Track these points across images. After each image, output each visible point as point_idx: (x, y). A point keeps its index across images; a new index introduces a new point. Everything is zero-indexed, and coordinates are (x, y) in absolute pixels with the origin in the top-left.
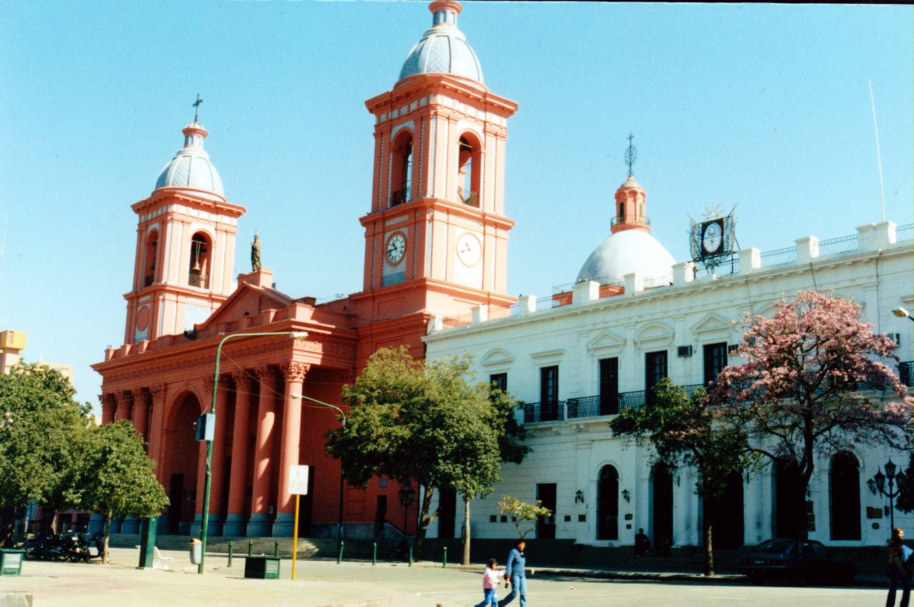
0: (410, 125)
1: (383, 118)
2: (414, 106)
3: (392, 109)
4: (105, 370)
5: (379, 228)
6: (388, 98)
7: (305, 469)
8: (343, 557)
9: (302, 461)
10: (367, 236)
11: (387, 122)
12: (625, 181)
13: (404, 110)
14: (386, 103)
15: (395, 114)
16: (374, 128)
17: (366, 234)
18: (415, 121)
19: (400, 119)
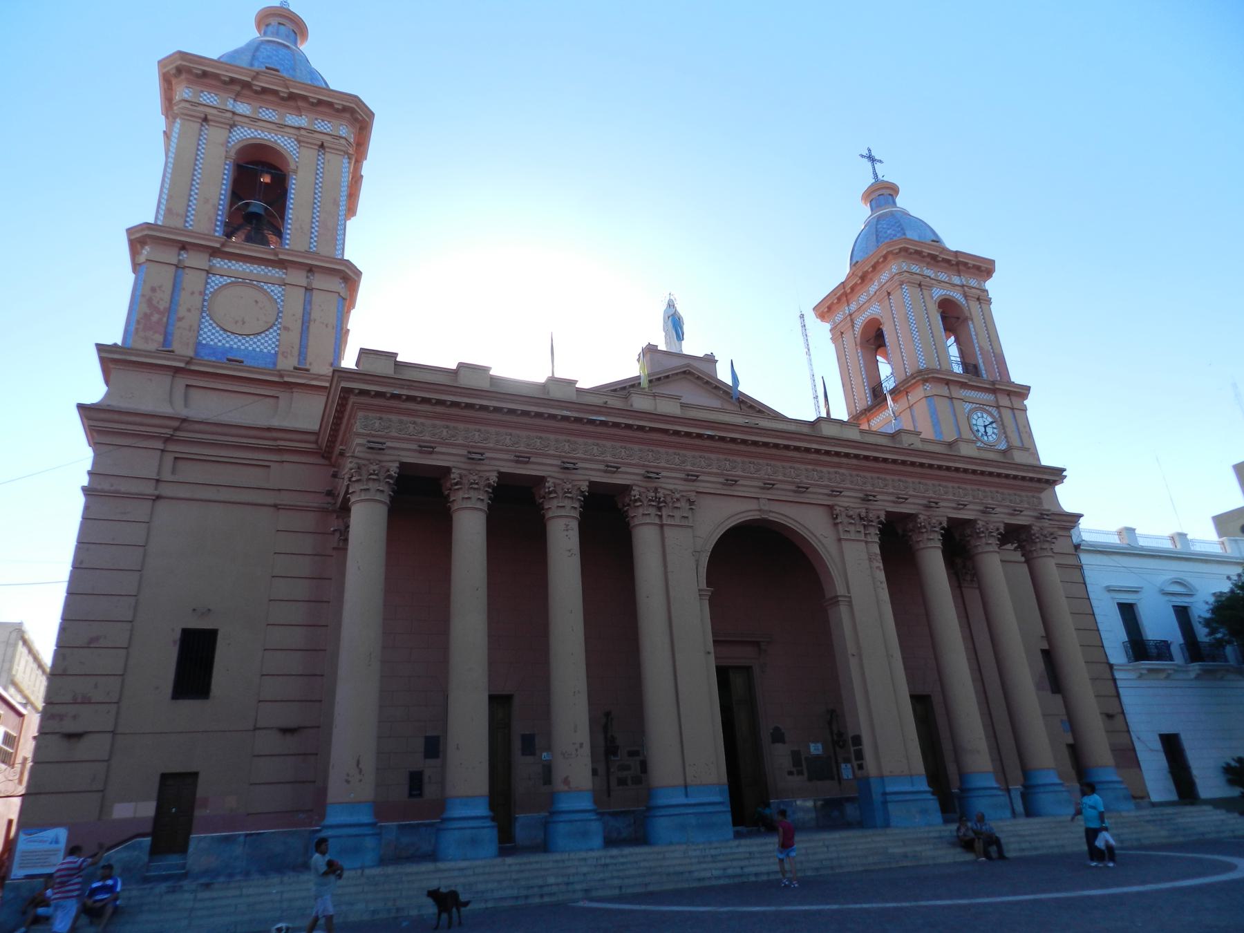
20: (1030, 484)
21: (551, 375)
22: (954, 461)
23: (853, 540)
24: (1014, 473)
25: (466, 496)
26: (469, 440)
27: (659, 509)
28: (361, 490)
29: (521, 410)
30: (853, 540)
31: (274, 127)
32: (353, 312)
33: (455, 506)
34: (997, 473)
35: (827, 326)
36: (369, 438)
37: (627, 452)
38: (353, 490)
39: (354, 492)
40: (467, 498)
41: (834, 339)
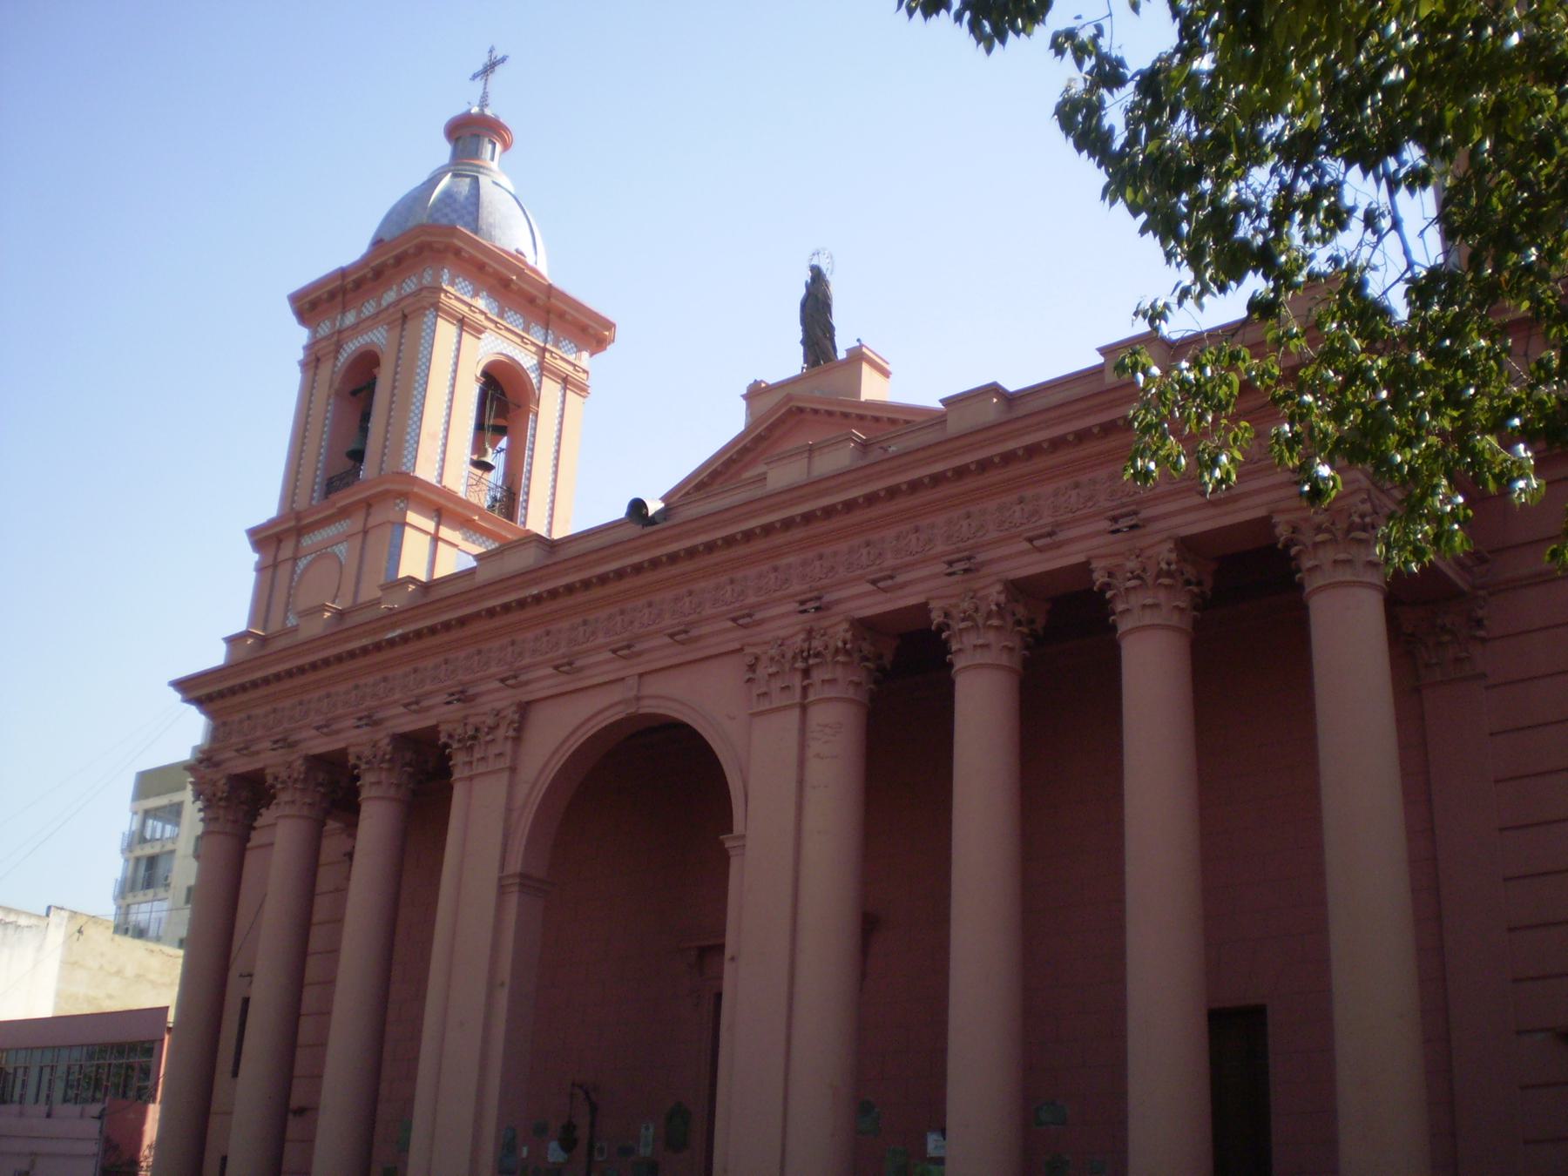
0: (378, 337)
1: (325, 329)
2: (390, 296)
3: (344, 310)
4: (221, 695)
5: (287, 551)
6: (338, 283)
7: (1106, 123)
8: (149, 1049)
9: (1112, 129)
10: (260, 569)
11: (332, 335)
12: (1079, 27)
13: (369, 308)
14: (332, 295)
15: (350, 318)
16: (302, 351)
17: (258, 563)
18: (388, 324)
19: (356, 328)
20: (675, 570)
21: (429, 537)
22: (349, 639)
23: (778, 709)
24: (862, 493)
25: (1342, 556)
26: (1006, 526)
27: (471, 748)
28: (975, 646)
29: (999, 454)
30: (778, 709)
32: (800, 336)
33: (1313, 582)
34: (723, 538)
35: (302, 335)
36: (272, 739)
38: (959, 646)
39: (960, 650)
40: (982, 646)
41: (304, 365)
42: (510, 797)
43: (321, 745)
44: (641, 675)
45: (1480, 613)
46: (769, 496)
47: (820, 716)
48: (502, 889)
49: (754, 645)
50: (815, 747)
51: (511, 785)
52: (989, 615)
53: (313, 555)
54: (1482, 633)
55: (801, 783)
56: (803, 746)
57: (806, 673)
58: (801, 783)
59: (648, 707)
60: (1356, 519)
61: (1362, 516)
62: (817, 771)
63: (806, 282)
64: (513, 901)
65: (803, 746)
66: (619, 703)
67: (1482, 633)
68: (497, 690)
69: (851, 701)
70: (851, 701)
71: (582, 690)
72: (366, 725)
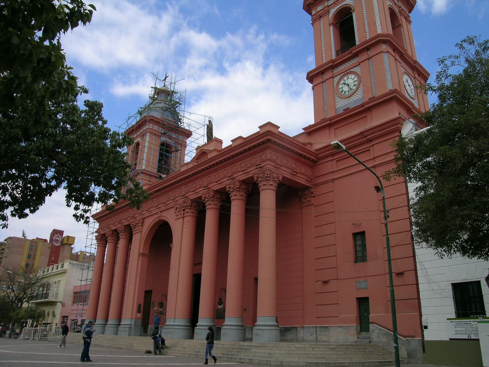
31: (333, 5)
37: (245, 164)
42: (141, 237)
43: (194, 196)
44: (161, 212)
45: (312, 191)
46: (261, 135)
47: (186, 219)
48: (139, 256)
49: (176, 205)
50: (185, 226)
51: (141, 235)
52: (211, 198)
53: (343, 74)
54: (313, 195)
55: (182, 233)
56: (183, 226)
57: (184, 210)
58: (182, 233)
59: (162, 218)
60: (266, 175)
61: (267, 175)
62: (185, 231)
63: (50, 195)
64: (141, 258)
65: (183, 226)
66: (158, 217)
67: (313, 195)
68: (146, 213)
69: (126, 238)
70: (126, 238)
71: (153, 215)
72: (207, 189)
